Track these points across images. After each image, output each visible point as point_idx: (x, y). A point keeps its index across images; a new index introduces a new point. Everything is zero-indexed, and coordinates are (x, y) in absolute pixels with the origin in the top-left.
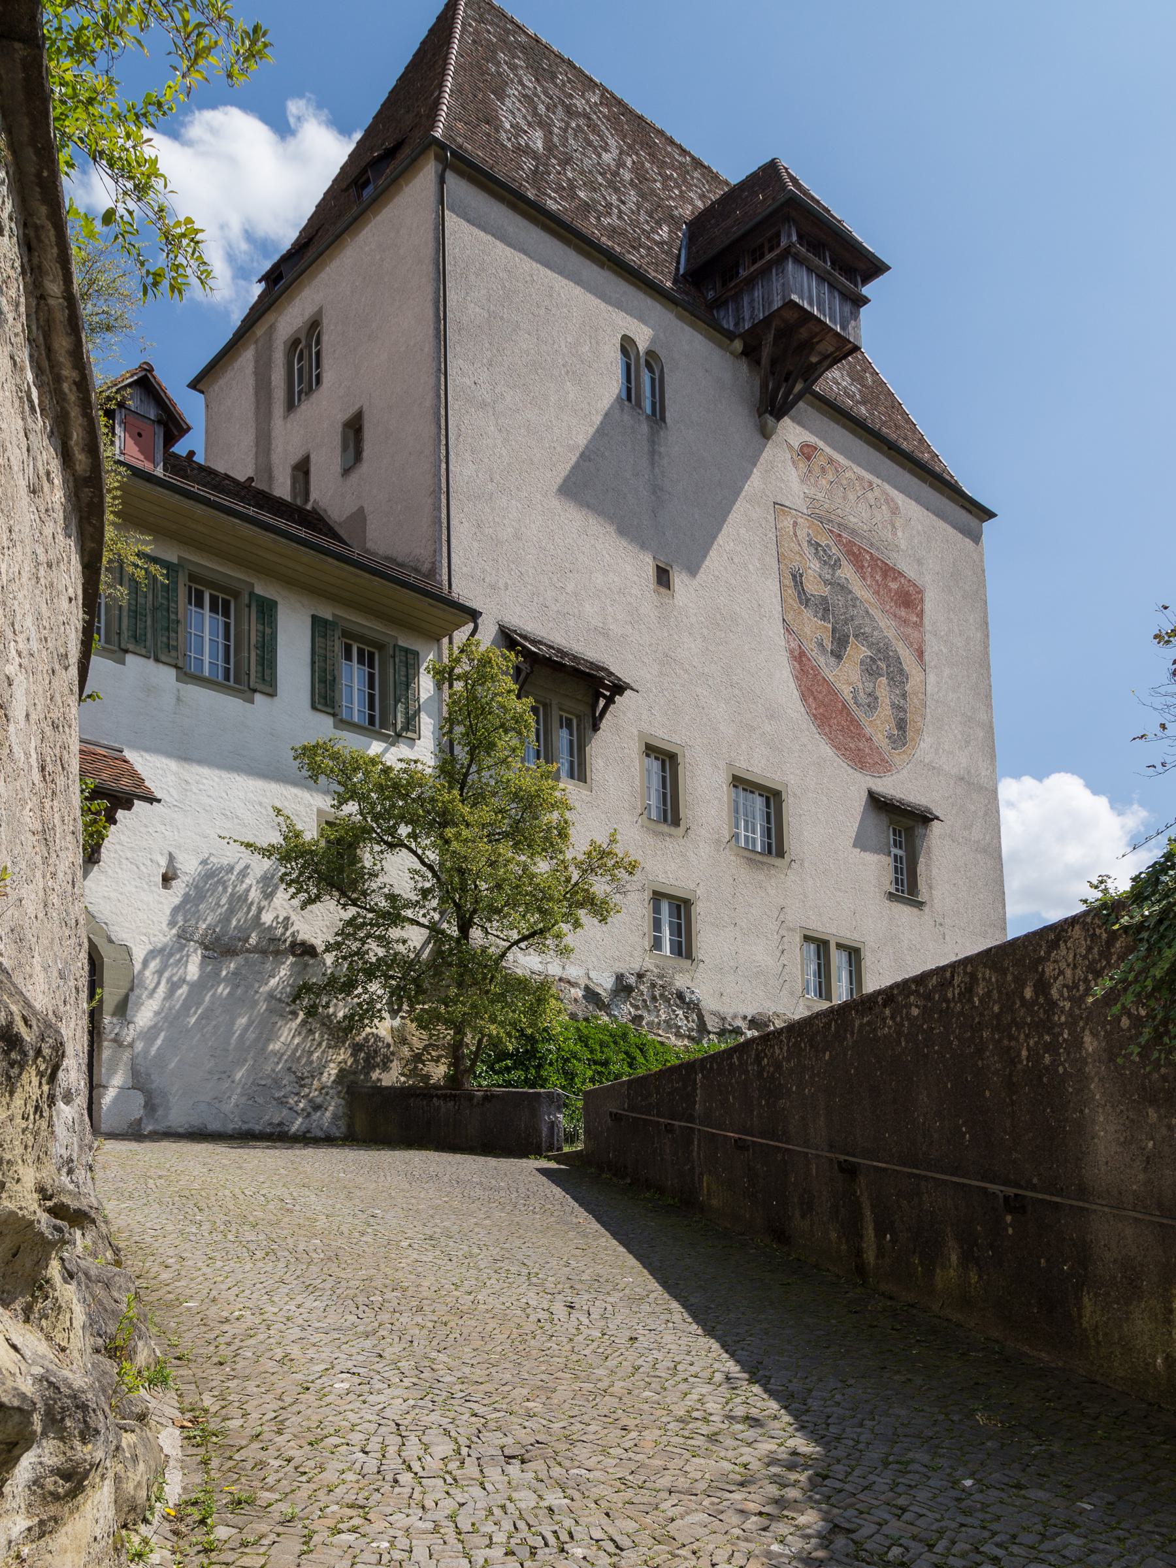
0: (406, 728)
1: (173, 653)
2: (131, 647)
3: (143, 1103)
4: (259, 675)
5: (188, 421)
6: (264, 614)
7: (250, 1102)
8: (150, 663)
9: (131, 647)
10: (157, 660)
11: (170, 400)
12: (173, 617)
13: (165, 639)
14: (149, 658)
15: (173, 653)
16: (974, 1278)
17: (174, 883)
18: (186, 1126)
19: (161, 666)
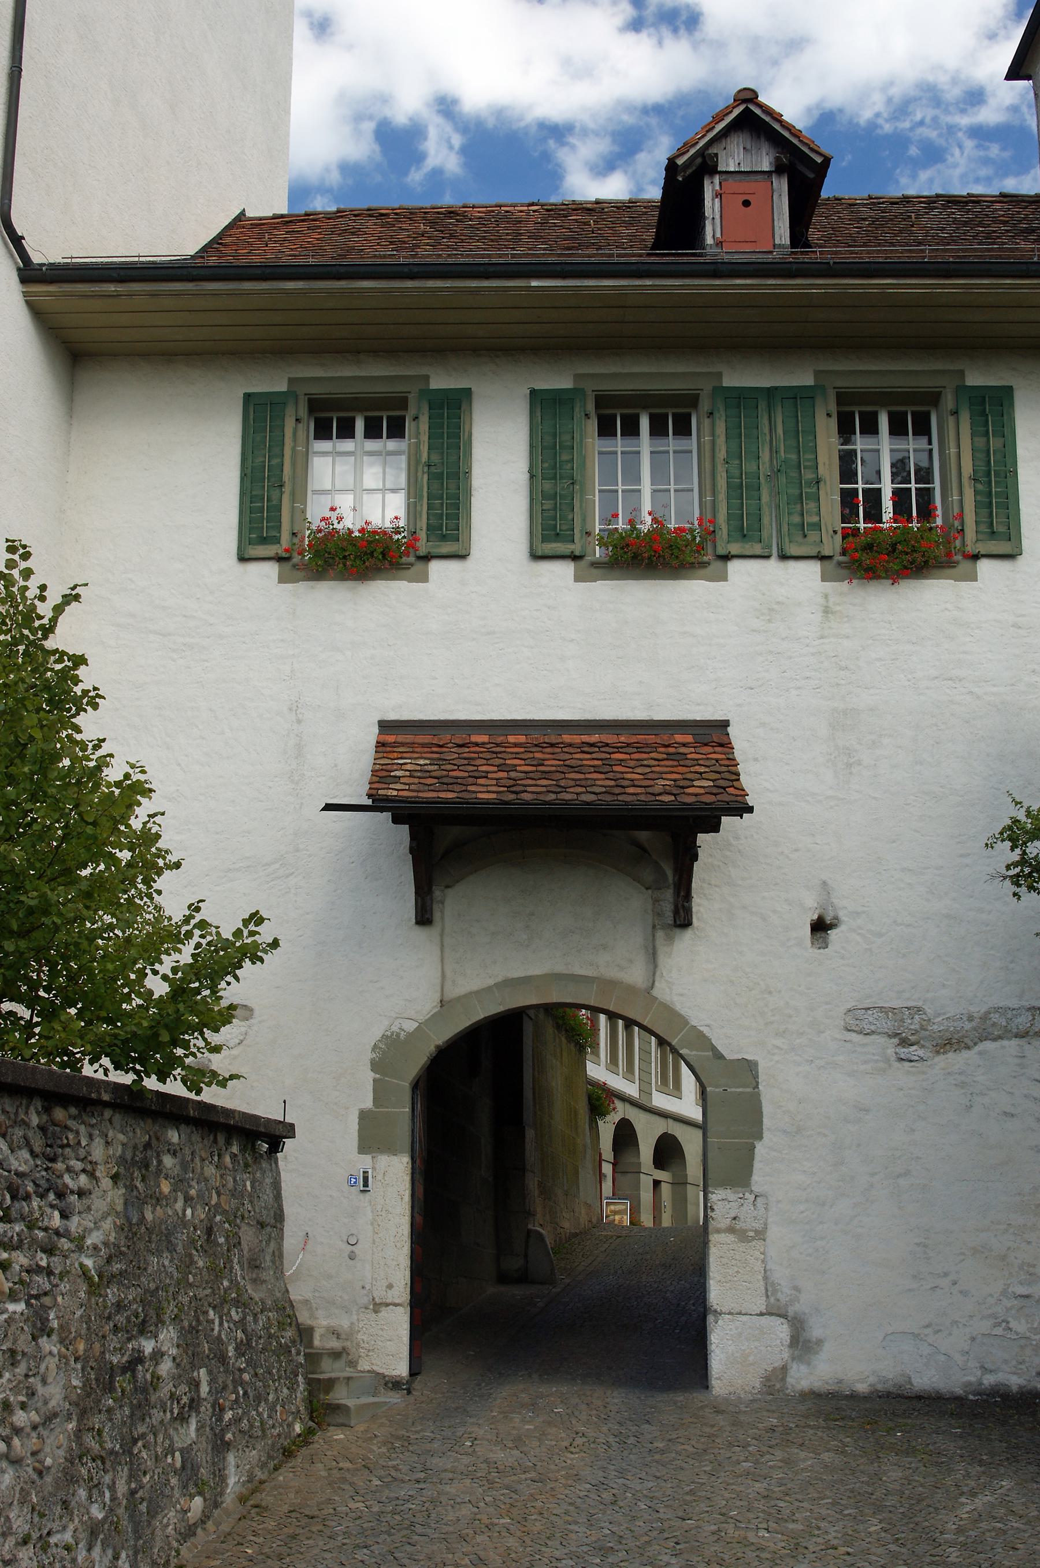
0: (854, 560)
1: (813, 536)
2: (734, 548)
3: (787, 1340)
4: (984, 528)
5: (824, 150)
6: (984, 414)
7: (999, 1331)
8: (773, 567)
9: (734, 548)
10: (784, 557)
11: (12, 256)
12: (808, 475)
13: (796, 519)
14: (768, 557)
15: (813, 536)
16: (189, 1212)
17: (833, 934)
18: (872, 1380)
19: (792, 564)
